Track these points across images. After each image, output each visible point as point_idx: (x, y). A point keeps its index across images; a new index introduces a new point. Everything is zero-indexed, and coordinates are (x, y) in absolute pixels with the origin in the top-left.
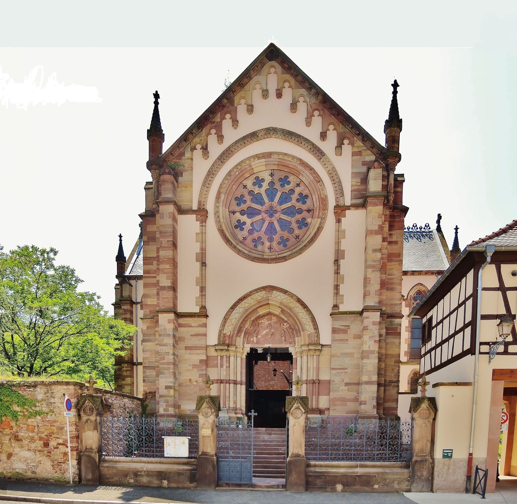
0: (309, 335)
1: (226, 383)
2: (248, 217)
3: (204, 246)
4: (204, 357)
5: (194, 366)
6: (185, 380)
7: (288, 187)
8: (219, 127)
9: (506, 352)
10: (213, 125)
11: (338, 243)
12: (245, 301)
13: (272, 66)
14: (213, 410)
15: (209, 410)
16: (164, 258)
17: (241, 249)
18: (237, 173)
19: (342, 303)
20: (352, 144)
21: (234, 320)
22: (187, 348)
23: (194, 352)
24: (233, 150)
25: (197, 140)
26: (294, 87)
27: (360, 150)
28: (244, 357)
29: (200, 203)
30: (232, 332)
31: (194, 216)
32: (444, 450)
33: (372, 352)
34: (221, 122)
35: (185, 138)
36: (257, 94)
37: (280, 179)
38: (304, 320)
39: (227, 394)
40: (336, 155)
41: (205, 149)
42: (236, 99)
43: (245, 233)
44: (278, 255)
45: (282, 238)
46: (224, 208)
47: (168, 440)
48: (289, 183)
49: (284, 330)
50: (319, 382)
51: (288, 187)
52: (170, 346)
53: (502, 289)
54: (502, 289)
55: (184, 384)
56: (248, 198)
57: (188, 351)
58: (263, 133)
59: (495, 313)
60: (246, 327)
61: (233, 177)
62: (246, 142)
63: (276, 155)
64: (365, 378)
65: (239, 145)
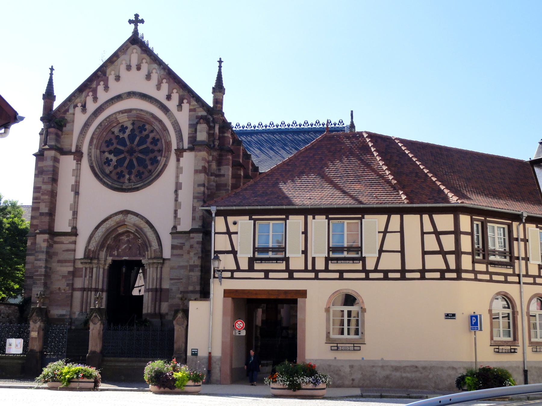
0: (155, 251)
1: (88, 291)
2: (115, 156)
3: (78, 179)
4: (71, 269)
5: (64, 277)
6: (55, 288)
7: (145, 133)
8: (95, 92)
9: (232, 277)
10: (91, 90)
11: (177, 177)
12: (107, 222)
13: (134, 49)
14: (40, 318)
15: (38, 318)
16: (45, 191)
17: (106, 181)
18: (106, 124)
19: (179, 224)
20: (189, 102)
21: (97, 238)
22: (59, 261)
23: (64, 264)
24: (104, 107)
25: (78, 100)
26: (149, 63)
27: (194, 107)
28: (106, 267)
29: (77, 146)
30: (96, 248)
31: (72, 157)
32: (360, 350)
33: (196, 266)
34: (96, 88)
35: (70, 99)
36: (123, 67)
37: (139, 127)
38: (151, 238)
39: (89, 300)
40: (178, 111)
41: (84, 107)
42: (108, 71)
43: (111, 168)
44: (134, 185)
45: (138, 171)
46: (95, 150)
47: (20, 341)
48: (145, 130)
49: (139, 245)
50: (161, 289)
51: (145, 133)
52: (43, 261)
53: (229, 233)
54: (229, 233)
55: (55, 292)
56: (114, 141)
57: (60, 264)
58: (125, 95)
59: (224, 250)
60: (108, 243)
61: (103, 126)
62: (113, 102)
63: (135, 111)
64: (191, 288)
65: (108, 104)
